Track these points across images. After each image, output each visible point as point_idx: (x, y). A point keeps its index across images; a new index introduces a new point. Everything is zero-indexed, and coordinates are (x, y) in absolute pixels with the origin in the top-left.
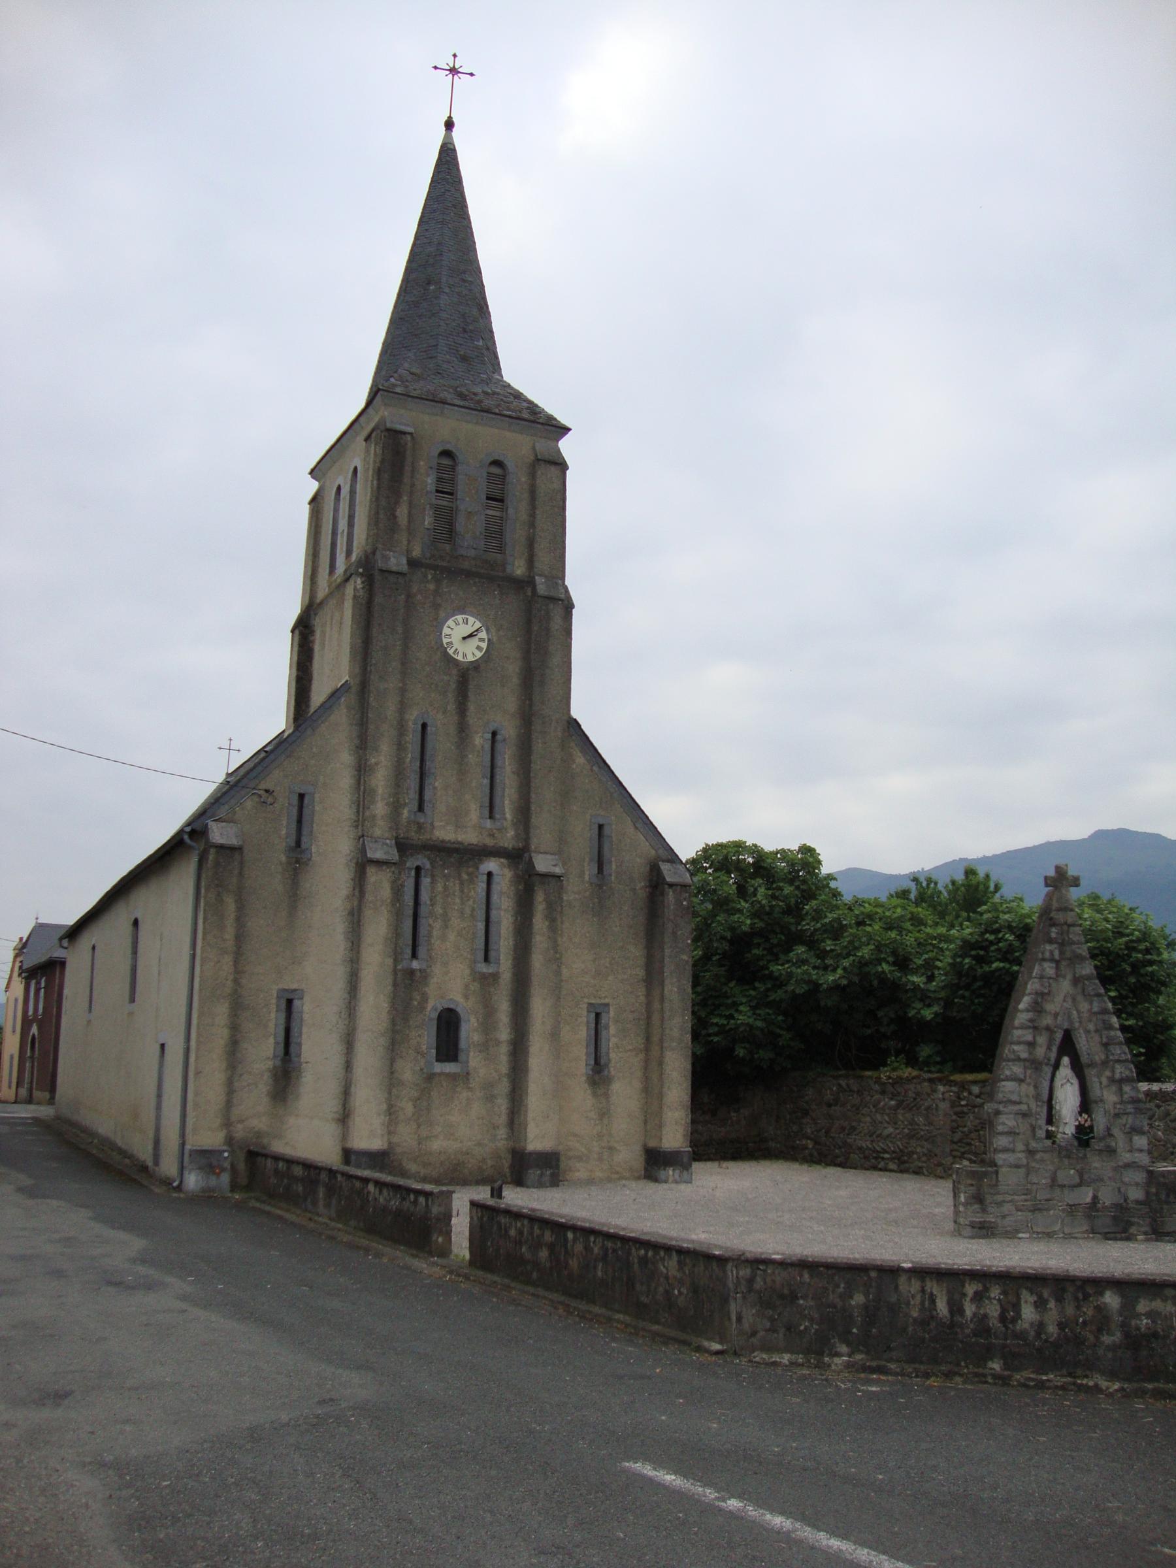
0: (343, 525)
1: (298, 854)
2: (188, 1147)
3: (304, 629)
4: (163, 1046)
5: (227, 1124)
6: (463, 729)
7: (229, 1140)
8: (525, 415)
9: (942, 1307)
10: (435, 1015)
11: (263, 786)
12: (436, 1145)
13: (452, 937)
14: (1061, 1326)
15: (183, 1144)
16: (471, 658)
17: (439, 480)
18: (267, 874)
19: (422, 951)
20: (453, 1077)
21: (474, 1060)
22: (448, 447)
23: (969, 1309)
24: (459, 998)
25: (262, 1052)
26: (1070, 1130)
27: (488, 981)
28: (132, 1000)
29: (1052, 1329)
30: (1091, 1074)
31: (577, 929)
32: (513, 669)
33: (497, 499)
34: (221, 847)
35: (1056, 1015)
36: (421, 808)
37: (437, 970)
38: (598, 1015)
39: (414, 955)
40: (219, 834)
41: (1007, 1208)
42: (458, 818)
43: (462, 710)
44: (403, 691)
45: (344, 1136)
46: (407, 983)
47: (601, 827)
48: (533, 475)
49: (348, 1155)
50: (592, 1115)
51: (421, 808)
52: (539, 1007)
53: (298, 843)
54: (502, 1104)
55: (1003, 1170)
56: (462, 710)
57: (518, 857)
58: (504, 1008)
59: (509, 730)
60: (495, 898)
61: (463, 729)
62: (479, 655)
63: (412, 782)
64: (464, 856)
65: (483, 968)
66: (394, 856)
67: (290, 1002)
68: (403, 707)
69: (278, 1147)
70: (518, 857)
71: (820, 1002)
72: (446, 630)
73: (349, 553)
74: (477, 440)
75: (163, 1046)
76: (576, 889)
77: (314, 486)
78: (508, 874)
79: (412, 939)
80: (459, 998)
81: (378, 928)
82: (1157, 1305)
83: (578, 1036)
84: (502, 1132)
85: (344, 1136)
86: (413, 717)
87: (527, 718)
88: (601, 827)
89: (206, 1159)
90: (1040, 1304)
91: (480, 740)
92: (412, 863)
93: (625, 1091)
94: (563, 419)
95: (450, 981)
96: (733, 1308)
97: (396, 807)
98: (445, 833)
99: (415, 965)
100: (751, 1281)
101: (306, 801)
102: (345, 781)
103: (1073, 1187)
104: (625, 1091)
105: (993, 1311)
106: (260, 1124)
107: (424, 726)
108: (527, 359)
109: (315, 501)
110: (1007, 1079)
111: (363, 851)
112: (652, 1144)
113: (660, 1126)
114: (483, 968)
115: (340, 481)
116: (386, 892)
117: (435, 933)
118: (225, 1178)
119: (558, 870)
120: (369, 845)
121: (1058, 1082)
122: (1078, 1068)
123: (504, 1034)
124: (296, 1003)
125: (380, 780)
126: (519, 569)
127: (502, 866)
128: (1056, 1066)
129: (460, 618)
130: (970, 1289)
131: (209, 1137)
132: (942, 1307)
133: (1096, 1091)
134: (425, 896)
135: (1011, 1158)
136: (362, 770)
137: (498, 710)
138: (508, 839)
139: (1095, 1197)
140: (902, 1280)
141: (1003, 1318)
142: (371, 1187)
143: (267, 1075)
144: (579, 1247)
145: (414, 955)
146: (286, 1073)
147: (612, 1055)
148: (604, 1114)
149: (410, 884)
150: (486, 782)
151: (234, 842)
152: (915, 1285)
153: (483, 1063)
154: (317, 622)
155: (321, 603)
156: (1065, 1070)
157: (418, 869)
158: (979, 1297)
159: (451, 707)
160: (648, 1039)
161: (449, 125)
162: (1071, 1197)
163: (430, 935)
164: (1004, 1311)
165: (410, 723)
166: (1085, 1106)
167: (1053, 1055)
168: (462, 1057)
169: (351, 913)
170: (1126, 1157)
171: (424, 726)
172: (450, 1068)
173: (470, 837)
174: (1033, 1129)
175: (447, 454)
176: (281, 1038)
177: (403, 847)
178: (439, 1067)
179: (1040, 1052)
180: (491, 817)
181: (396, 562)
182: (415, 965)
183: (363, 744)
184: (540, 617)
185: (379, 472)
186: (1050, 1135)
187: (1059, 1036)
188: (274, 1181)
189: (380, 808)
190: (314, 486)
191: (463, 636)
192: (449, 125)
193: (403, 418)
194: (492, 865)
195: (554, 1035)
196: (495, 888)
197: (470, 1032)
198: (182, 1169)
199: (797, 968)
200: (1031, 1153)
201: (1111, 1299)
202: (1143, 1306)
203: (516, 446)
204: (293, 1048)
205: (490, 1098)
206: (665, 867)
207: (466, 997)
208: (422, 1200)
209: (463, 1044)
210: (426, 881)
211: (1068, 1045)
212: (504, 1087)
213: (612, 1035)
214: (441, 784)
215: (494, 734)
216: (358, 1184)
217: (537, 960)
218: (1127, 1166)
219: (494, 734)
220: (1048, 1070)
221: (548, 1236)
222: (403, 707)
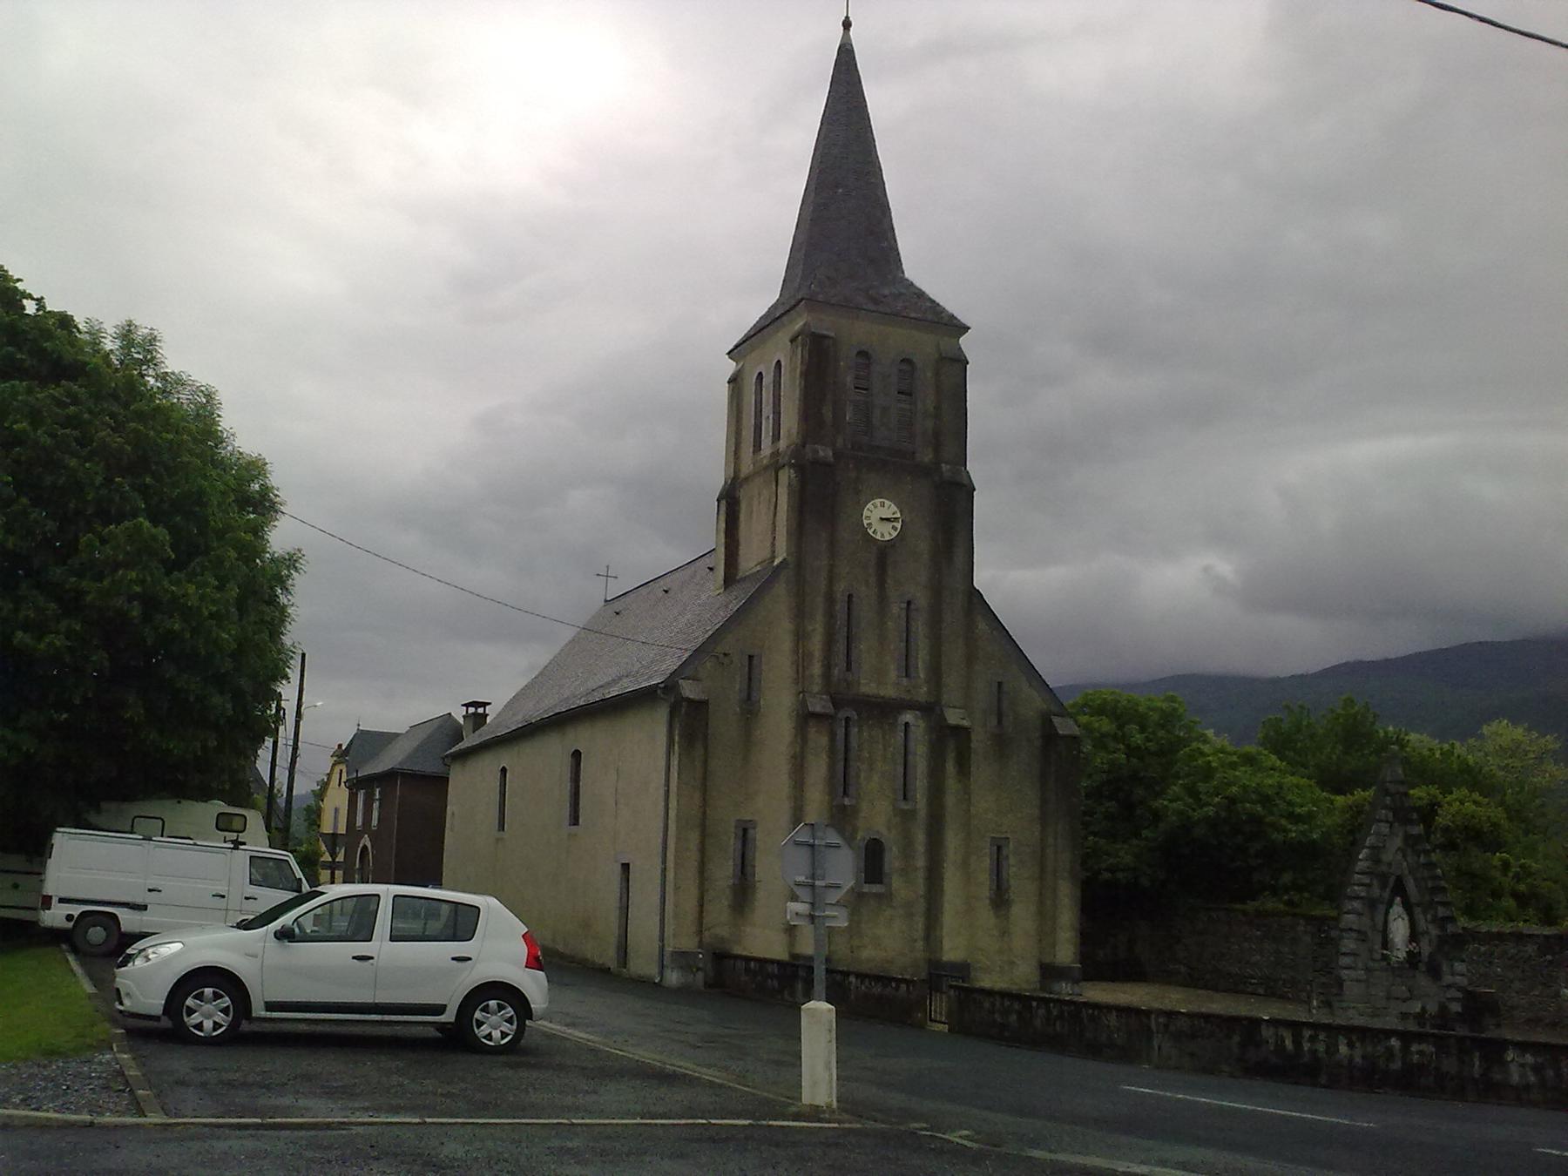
0: (767, 410)
1: (750, 708)
2: (669, 949)
3: (730, 500)
4: (626, 867)
5: (700, 932)
6: (882, 599)
7: (701, 944)
8: (930, 317)
9: (1288, 1043)
10: (863, 844)
11: (719, 649)
12: (866, 953)
13: (876, 778)
14: (1363, 1057)
15: (662, 949)
16: (887, 538)
17: (857, 377)
18: (724, 724)
19: (852, 790)
20: (878, 896)
21: (896, 882)
22: (863, 348)
23: (1306, 1046)
24: (884, 831)
25: (723, 873)
26: (1402, 955)
27: (907, 816)
28: (575, 820)
29: (1358, 1060)
30: (1417, 911)
31: (982, 771)
32: (923, 547)
33: (907, 393)
34: (689, 700)
35: (1390, 865)
36: (849, 668)
37: (864, 806)
38: (999, 848)
39: (845, 793)
40: (689, 690)
41: (1351, 1013)
42: (878, 676)
43: (882, 584)
44: (831, 568)
45: (792, 944)
46: (842, 816)
47: (1000, 684)
48: (937, 374)
49: (794, 956)
50: (995, 933)
51: (849, 668)
52: (953, 841)
53: (749, 697)
54: (920, 923)
55: (1347, 984)
56: (882, 584)
57: (930, 710)
58: (920, 838)
59: (922, 600)
60: (912, 745)
61: (882, 599)
62: (895, 534)
63: (841, 647)
64: (883, 710)
65: (905, 806)
66: (830, 709)
67: (745, 831)
68: (831, 580)
69: (738, 950)
70: (930, 710)
71: (1201, 846)
72: (866, 513)
73: (776, 437)
74: (891, 341)
75: (626, 867)
76: (980, 741)
77: (730, 367)
78: (922, 724)
79: (842, 783)
80: (884, 831)
81: (818, 769)
82: (1423, 1047)
83: (983, 866)
84: (920, 944)
85: (792, 944)
86: (841, 588)
87: (937, 591)
88: (1000, 684)
89: (683, 959)
90: (1351, 1045)
91: (896, 609)
92: (842, 714)
93: (1022, 914)
94: (963, 318)
95: (876, 816)
96: (1155, 1043)
97: (828, 667)
98: (868, 687)
99: (847, 801)
100: (1166, 1026)
101: (755, 662)
102: (786, 644)
103: (1404, 1001)
104: (1022, 914)
105: (1321, 1048)
106: (723, 932)
107: (850, 596)
108: (929, 253)
109: (734, 380)
110: (1348, 913)
111: (803, 703)
112: (1047, 960)
113: (1054, 945)
114: (905, 806)
115: (761, 368)
116: (824, 740)
117: (863, 775)
118: (700, 975)
119: (965, 723)
120: (810, 700)
121: (1391, 917)
122: (1408, 907)
123: (921, 862)
124: (751, 832)
125: (816, 645)
126: (927, 457)
127: (916, 717)
128: (1390, 904)
129: (878, 501)
130: (1307, 1033)
131: (688, 943)
132: (1288, 1043)
133: (1422, 924)
134: (854, 743)
135: (1352, 974)
136: (800, 636)
137: (912, 581)
138: (922, 694)
139: (1423, 1008)
140: (1263, 1027)
141: (1327, 1052)
142: (852, 979)
143: (728, 891)
144: (1042, 1012)
145: (845, 793)
146: (743, 891)
147: (1012, 882)
148: (1004, 933)
149: (841, 732)
150: (903, 645)
151: (703, 697)
152: (1272, 1031)
153: (905, 887)
154: (743, 494)
155: (746, 479)
156: (1397, 909)
157: (847, 719)
158: (1313, 1039)
159: (873, 580)
160: (1042, 870)
161: (847, 24)
162: (1404, 1008)
163: (858, 776)
164: (1328, 1048)
165: (1256, 904)
166: (1414, 936)
167: (1386, 894)
168: (886, 880)
169: (794, 757)
170: (1448, 979)
171: (850, 596)
172: (876, 888)
173: (889, 692)
174: (1371, 951)
175: (863, 354)
176: (739, 862)
177: (837, 703)
178: (866, 888)
179: (1376, 892)
180: (907, 676)
181: (825, 453)
182: (847, 801)
183: (800, 614)
184: (949, 508)
185: (805, 375)
186: (1385, 958)
187: (1392, 880)
188: (744, 978)
189: (817, 669)
190: (730, 367)
191: (880, 516)
192: (847, 24)
193: (826, 324)
194: (908, 717)
195: (965, 864)
196: (912, 736)
197: (892, 859)
198: (662, 967)
199: (1173, 802)
200: (1368, 970)
201: (1394, 1042)
202: (1414, 1048)
203: (923, 345)
204: (749, 869)
205: (910, 916)
206: (1056, 720)
207: (889, 829)
208: (903, 987)
209: (886, 868)
210: (854, 730)
211: (1399, 889)
212: (921, 906)
213: (1012, 868)
214: (865, 648)
215: (909, 603)
216: (838, 977)
217: (950, 800)
218: (1449, 986)
219: (909, 603)
220: (1382, 908)
221: (1016, 1006)
222: (831, 580)
